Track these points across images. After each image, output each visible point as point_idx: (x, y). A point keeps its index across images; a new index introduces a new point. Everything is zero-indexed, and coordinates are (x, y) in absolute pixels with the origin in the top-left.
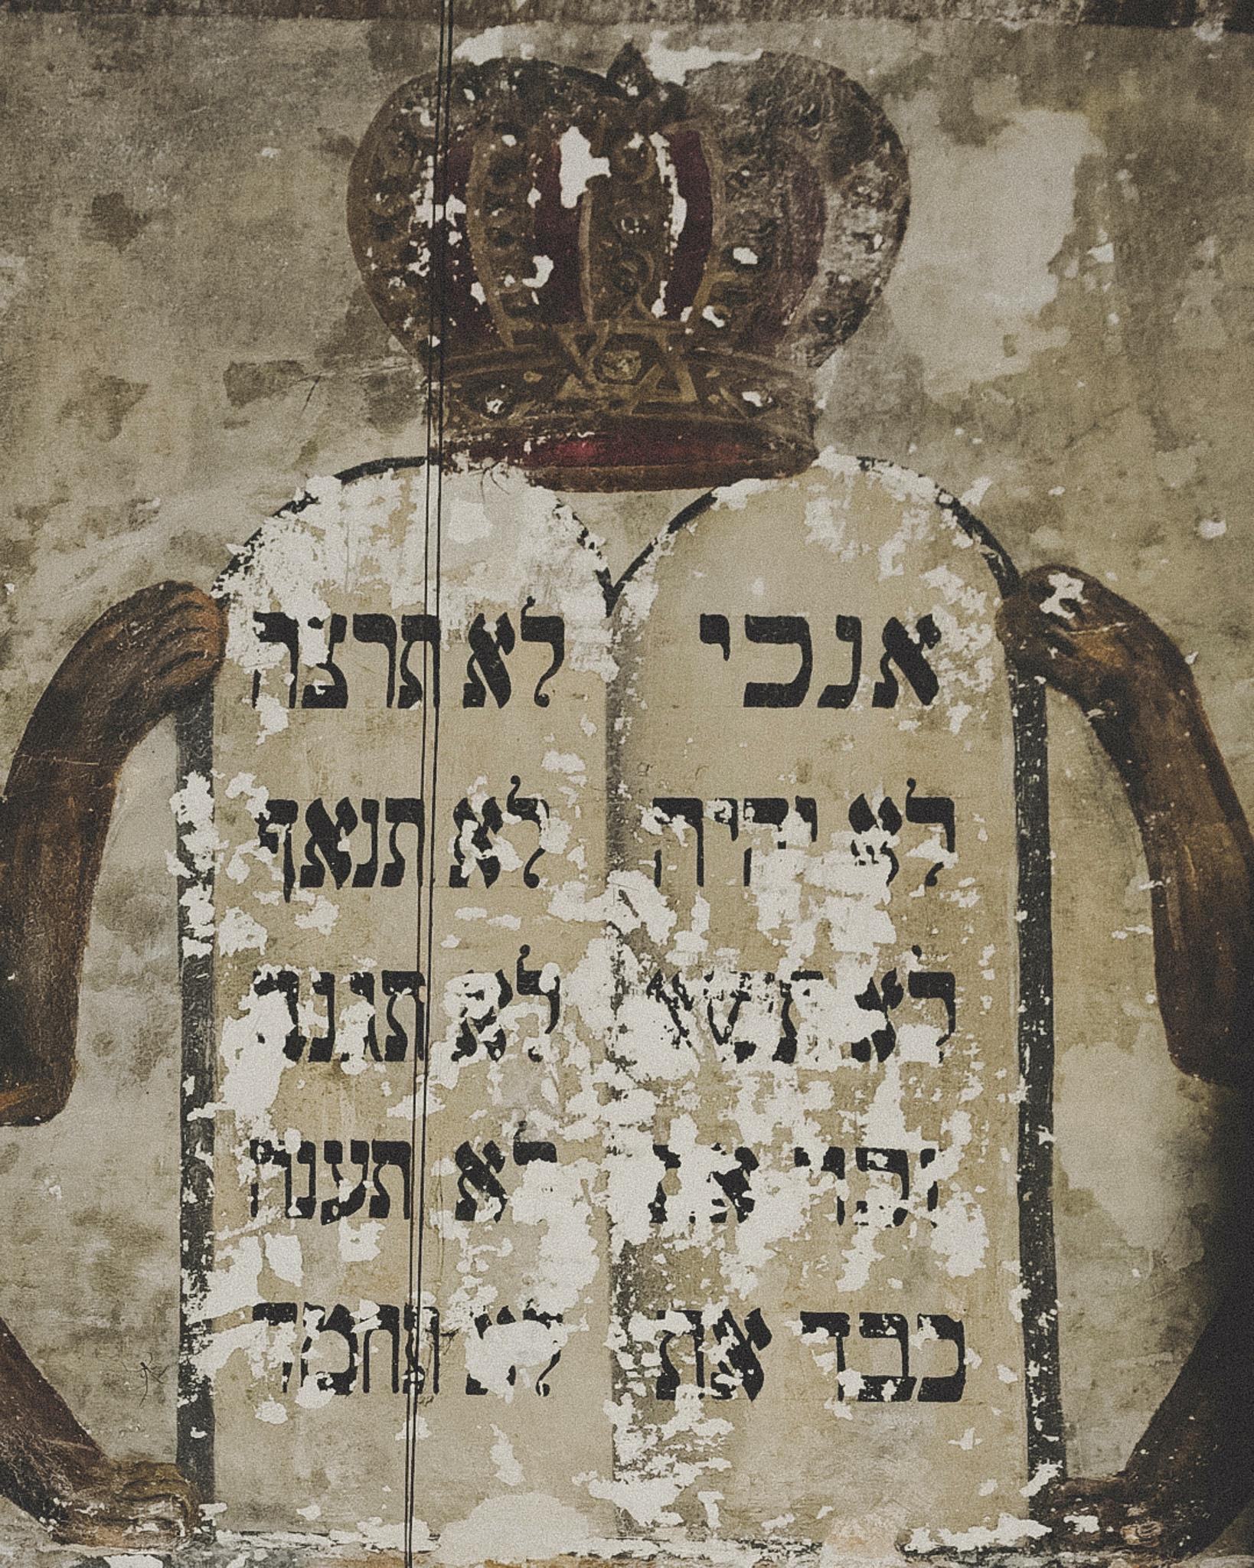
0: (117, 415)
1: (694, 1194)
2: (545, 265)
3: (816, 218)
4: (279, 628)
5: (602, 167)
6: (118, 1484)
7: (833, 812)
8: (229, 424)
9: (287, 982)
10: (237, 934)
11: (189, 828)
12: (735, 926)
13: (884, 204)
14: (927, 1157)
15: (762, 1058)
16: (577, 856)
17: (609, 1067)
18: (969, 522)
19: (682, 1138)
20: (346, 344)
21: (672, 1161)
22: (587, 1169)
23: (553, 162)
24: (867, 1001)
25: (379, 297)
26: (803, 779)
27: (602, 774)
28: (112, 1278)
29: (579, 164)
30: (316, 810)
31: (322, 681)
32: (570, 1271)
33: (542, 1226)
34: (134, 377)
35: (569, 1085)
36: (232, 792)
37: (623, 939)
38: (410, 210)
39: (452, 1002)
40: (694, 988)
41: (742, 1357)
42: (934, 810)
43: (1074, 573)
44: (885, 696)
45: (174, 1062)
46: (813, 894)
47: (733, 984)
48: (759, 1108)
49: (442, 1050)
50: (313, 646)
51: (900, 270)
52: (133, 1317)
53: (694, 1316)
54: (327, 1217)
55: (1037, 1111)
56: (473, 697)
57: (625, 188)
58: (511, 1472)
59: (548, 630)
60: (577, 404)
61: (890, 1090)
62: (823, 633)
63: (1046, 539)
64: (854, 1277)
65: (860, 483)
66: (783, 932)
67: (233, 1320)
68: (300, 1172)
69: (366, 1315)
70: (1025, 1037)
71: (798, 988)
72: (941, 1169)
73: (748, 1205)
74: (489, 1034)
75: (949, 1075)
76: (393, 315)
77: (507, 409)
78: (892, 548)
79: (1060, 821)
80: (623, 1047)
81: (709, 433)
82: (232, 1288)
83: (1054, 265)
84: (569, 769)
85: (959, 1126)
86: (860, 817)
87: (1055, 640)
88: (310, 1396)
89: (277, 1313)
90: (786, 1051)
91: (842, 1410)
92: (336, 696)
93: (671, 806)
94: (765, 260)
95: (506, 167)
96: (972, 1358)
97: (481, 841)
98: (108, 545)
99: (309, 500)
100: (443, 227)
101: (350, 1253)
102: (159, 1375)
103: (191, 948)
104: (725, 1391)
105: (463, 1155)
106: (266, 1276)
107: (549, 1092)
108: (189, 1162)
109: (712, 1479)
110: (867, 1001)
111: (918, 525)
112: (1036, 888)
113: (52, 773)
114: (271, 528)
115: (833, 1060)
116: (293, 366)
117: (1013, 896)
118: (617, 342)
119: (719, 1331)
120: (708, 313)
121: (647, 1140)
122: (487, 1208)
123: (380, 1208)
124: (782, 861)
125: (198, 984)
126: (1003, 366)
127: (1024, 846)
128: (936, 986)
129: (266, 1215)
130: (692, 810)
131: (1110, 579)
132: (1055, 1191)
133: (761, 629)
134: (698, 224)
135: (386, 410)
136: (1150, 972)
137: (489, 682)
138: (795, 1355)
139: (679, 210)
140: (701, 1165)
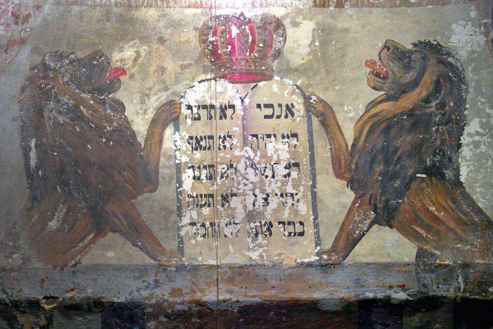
0: (163, 72)
1: (260, 201)
2: (230, 47)
3: (272, 39)
4: (190, 107)
5: (238, 31)
6: (168, 255)
7: (279, 136)
8: (181, 74)
9: (193, 167)
10: (185, 159)
11: (176, 141)
12: (264, 156)
13: (282, 36)
14: (297, 194)
15: (269, 178)
16: (238, 144)
17: (245, 180)
18: (298, 87)
19: (257, 192)
20: (199, 60)
21: (256, 196)
22: (242, 198)
23: (230, 32)
24: (286, 168)
25: (204, 52)
26: (274, 130)
27: (242, 130)
28: (166, 218)
29: (235, 31)
30: (196, 138)
31: (197, 116)
32: (240, 215)
33: (235, 208)
34: (166, 66)
35: (239, 184)
36: (183, 135)
37: (246, 158)
38: (208, 39)
39: (221, 168)
40: (258, 166)
41: (269, 230)
42: (295, 135)
43: (315, 96)
44: (286, 117)
45: (174, 181)
46: (276, 150)
47: (264, 165)
48: (269, 187)
49: (219, 178)
50: (195, 110)
51: (285, 47)
52: (170, 225)
53: (260, 223)
54: (201, 208)
55: (314, 186)
56: (221, 118)
57: (242, 34)
58: (232, 251)
59: (232, 107)
60: (236, 70)
61: (290, 183)
62: (276, 107)
63: (310, 90)
64: (286, 215)
65: (281, 81)
66: (272, 156)
67: (186, 225)
68: (196, 199)
69: (208, 224)
70: (311, 173)
71: (275, 166)
72: (299, 196)
73: (268, 203)
74: (226, 175)
75: (300, 179)
76: (206, 55)
77: (225, 71)
78: (286, 92)
79: (315, 136)
80: (247, 177)
81: (257, 74)
82: (186, 220)
83: (309, 46)
84: (237, 130)
85: (301, 188)
86: (283, 137)
87: (312, 107)
88: (199, 238)
89: (193, 224)
90: (273, 177)
91: (285, 238)
92: (199, 119)
93: (253, 136)
94: (264, 46)
95: (222, 32)
96: (305, 229)
97: (223, 142)
98: (161, 94)
99: (194, 86)
100: (213, 41)
101: (205, 213)
102: (174, 235)
103: (177, 162)
104: (266, 235)
105: (222, 196)
106: (191, 217)
107: (236, 185)
108: (178, 198)
109: (265, 251)
110: (286, 168)
111: (290, 88)
112: (312, 147)
113: (153, 132)
114: (188, 90)
115: (281, 178)
116: (190, 64)
117: (308, 149)
118: (242, 59)
119: (265, 225)
120: (256, 54)
121: (251, 193)
122: (227, 205)
123: (209, 206)
124: (271, 146)
125: (179, 169)
126: (302, 62)
127: (309, 141)
128: (297, 165)
129: (191, 207)
130: (256, 136)
131: (321, 96)
132: (317, 200)
133: (266, 106)
134: (253, 41)
135: (205, 72)
136: (330, 162)
137: (223, 116)
138: (277, 229)
139: (250, 38)
140: (261, 196)
